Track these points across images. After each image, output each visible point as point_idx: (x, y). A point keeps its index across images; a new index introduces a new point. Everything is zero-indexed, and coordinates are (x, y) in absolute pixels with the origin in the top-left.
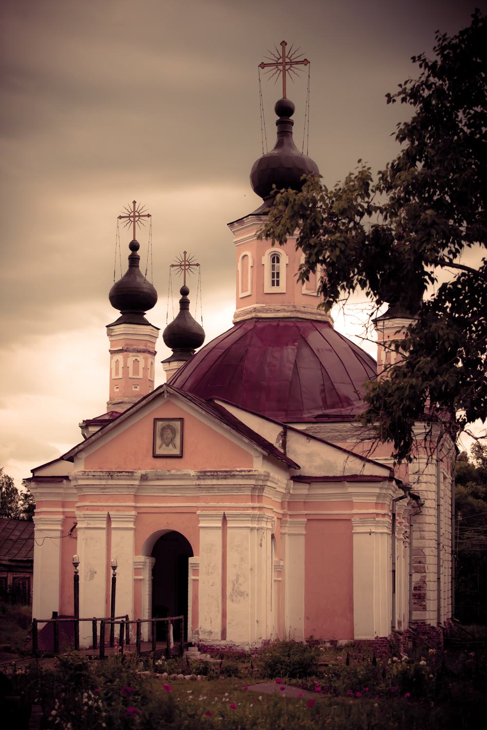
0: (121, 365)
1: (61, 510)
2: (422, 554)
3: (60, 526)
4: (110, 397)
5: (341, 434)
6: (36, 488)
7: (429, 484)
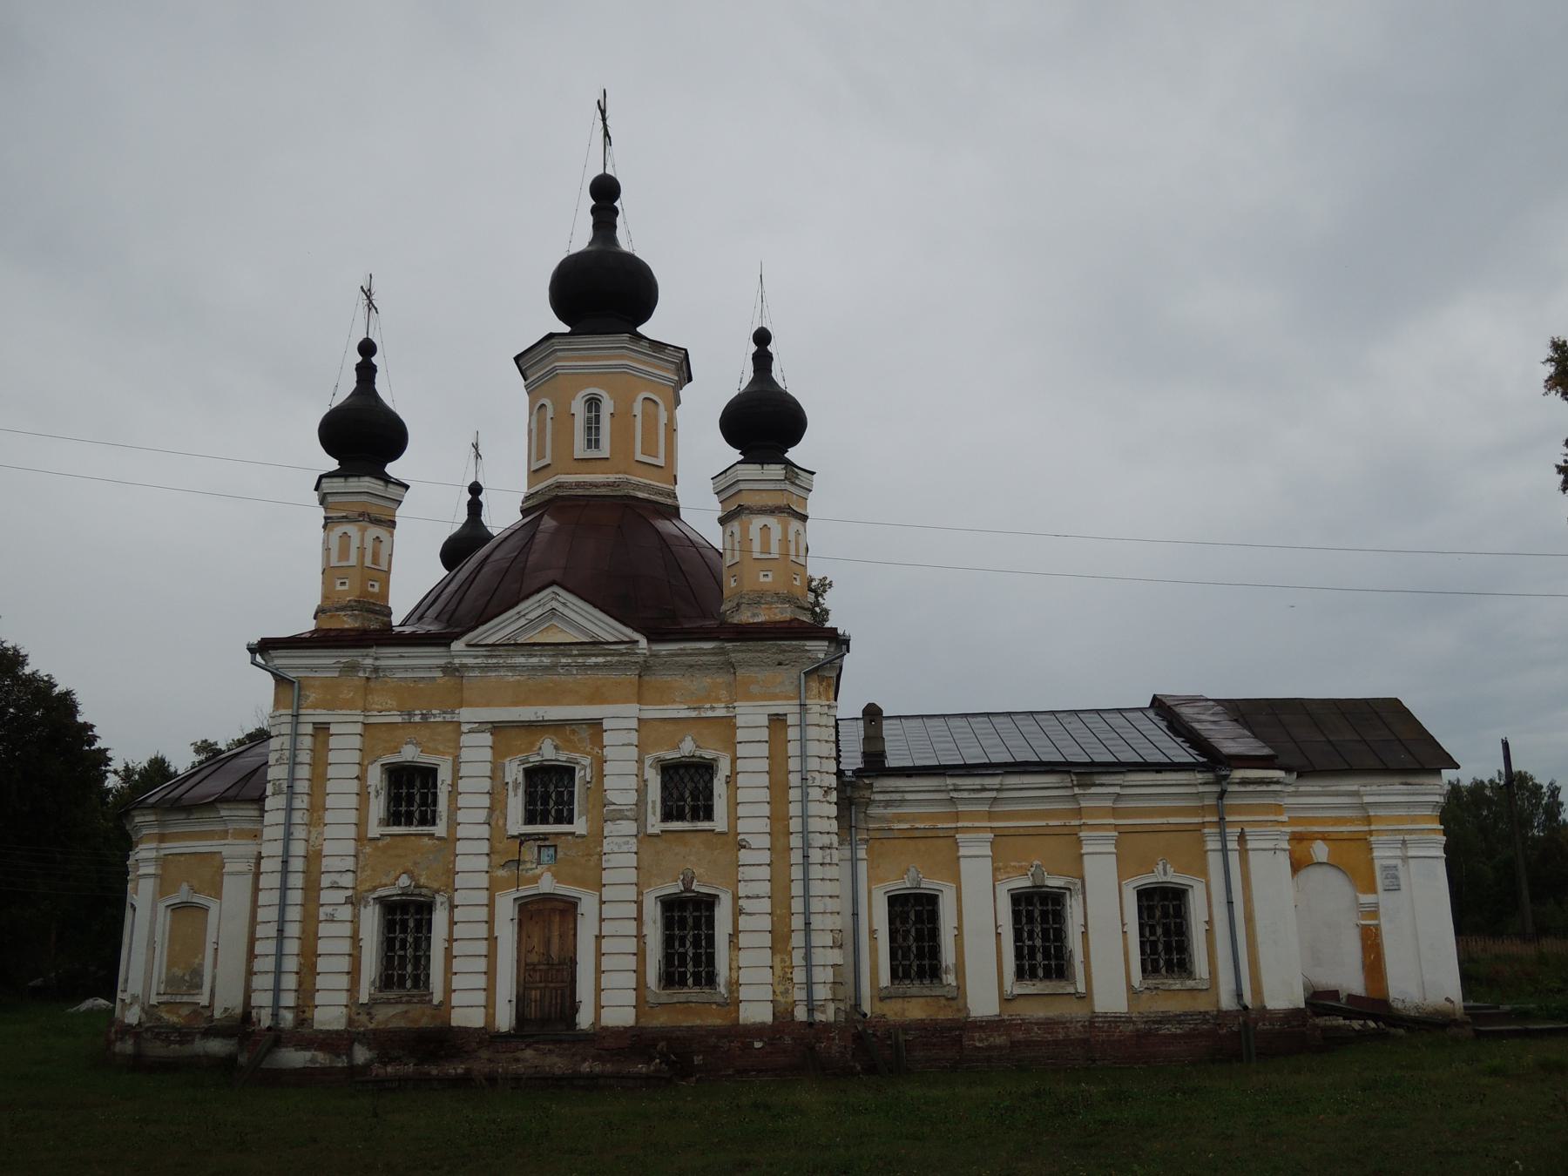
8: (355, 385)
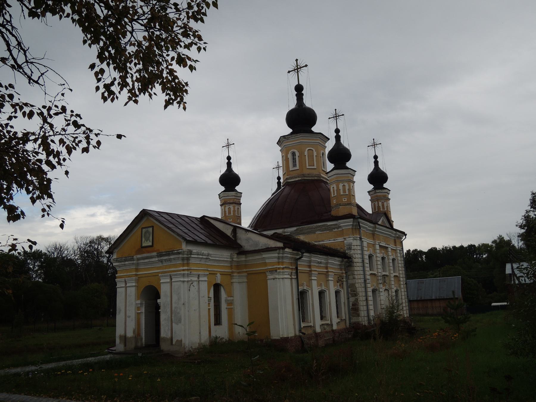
3: (332, 278)
7: (356, 250)
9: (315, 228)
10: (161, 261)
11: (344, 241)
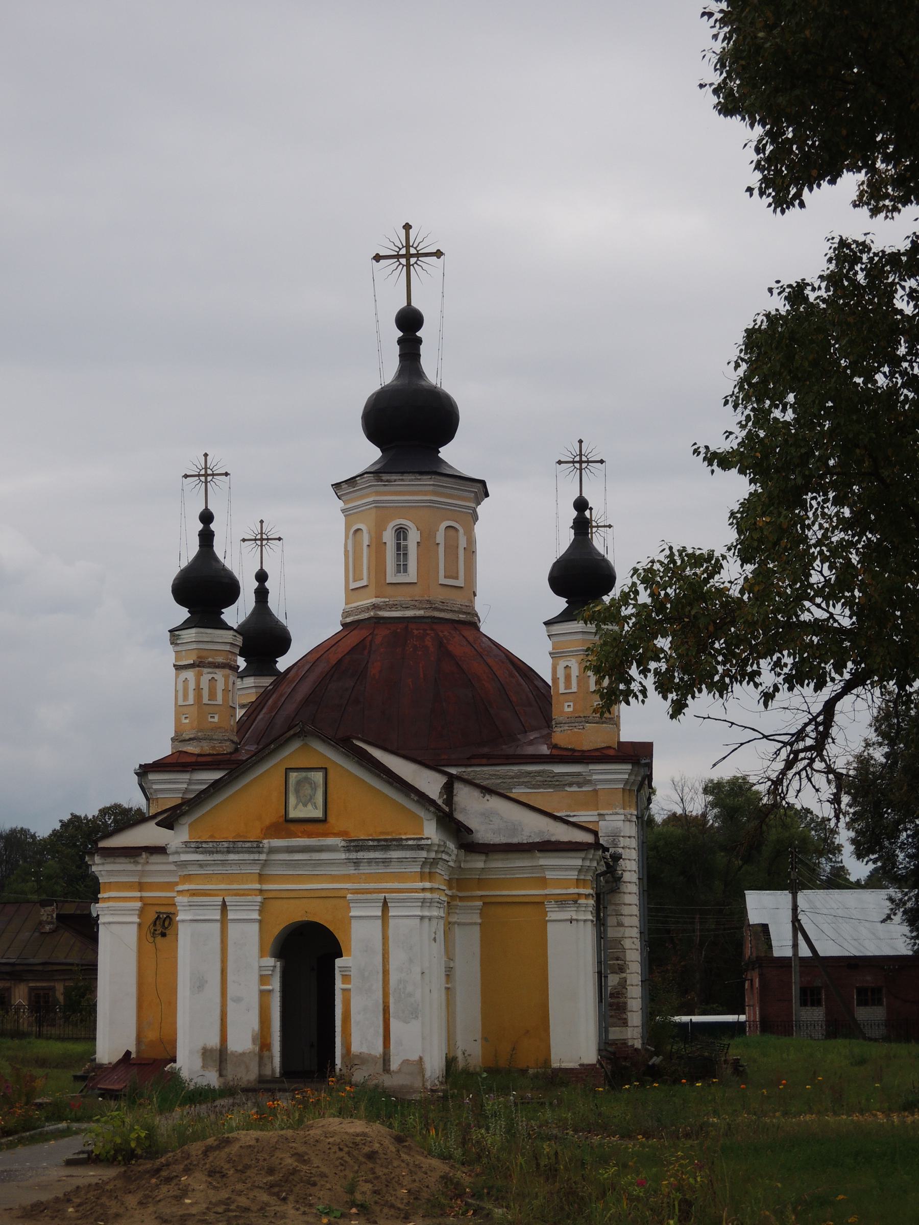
0: (192, 685)
1: (138, 894)
2: (620, 946)
4: (175, 731)
5: (504, 781)
6: (103, 864)
7: (627, 850)
8: (254, 604)
9: (513, 778)
10: (355, 863)
11: (598, 822)
